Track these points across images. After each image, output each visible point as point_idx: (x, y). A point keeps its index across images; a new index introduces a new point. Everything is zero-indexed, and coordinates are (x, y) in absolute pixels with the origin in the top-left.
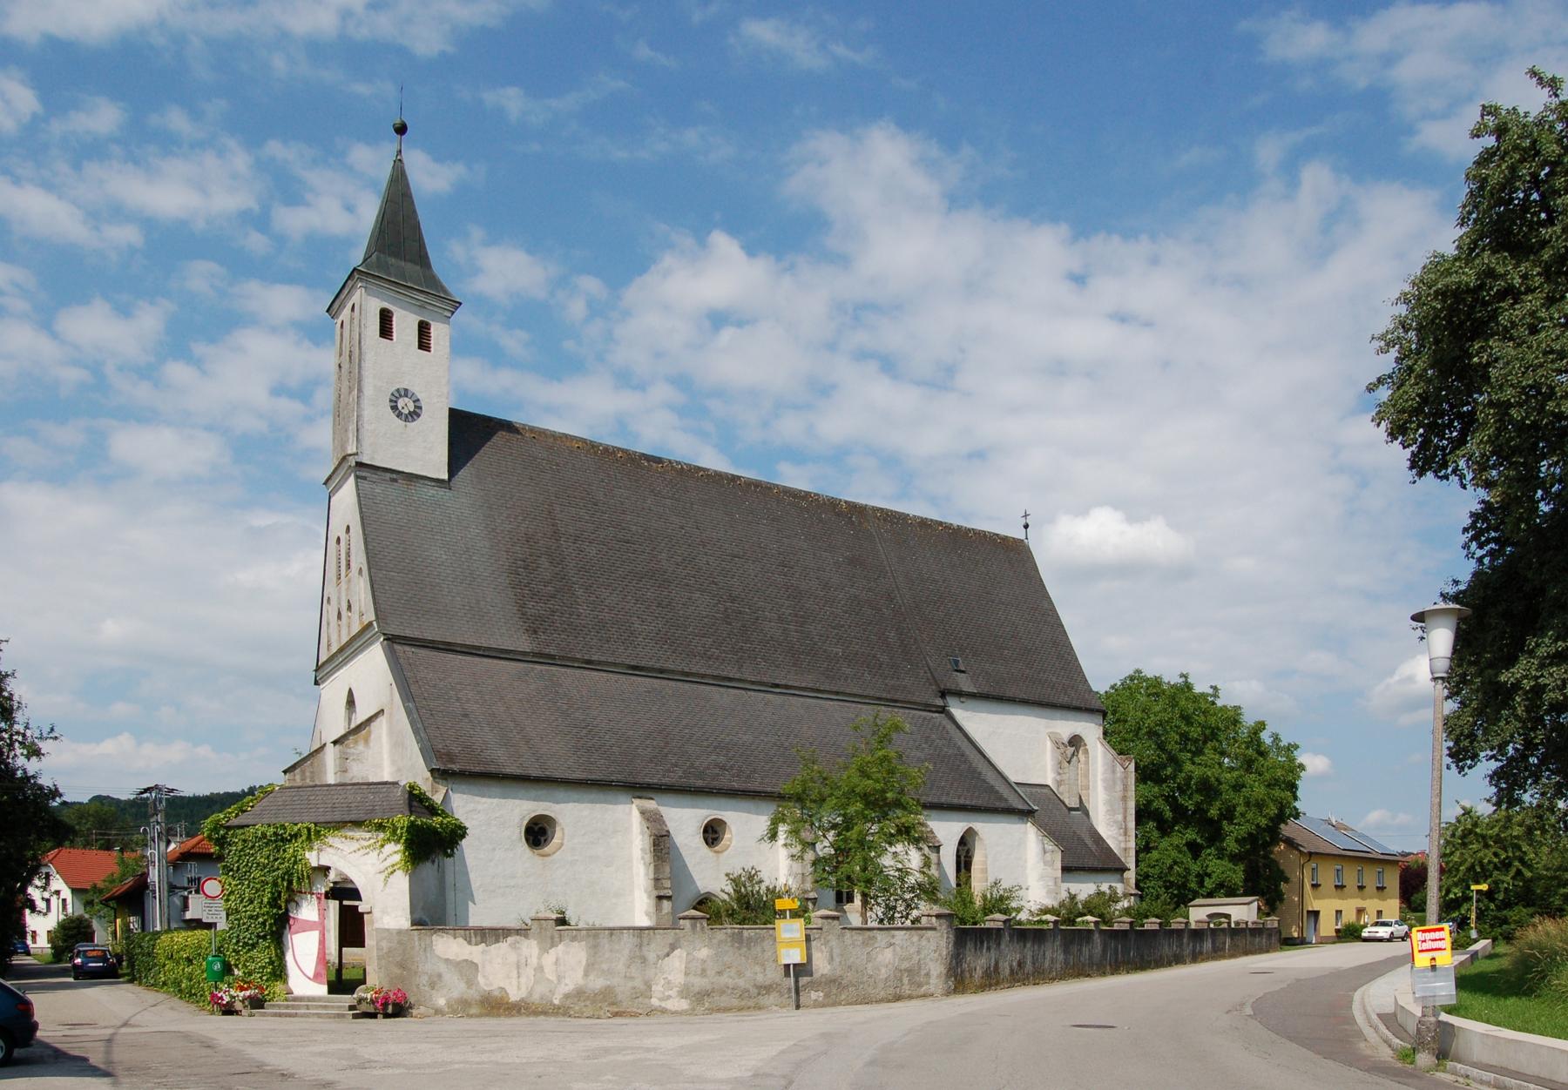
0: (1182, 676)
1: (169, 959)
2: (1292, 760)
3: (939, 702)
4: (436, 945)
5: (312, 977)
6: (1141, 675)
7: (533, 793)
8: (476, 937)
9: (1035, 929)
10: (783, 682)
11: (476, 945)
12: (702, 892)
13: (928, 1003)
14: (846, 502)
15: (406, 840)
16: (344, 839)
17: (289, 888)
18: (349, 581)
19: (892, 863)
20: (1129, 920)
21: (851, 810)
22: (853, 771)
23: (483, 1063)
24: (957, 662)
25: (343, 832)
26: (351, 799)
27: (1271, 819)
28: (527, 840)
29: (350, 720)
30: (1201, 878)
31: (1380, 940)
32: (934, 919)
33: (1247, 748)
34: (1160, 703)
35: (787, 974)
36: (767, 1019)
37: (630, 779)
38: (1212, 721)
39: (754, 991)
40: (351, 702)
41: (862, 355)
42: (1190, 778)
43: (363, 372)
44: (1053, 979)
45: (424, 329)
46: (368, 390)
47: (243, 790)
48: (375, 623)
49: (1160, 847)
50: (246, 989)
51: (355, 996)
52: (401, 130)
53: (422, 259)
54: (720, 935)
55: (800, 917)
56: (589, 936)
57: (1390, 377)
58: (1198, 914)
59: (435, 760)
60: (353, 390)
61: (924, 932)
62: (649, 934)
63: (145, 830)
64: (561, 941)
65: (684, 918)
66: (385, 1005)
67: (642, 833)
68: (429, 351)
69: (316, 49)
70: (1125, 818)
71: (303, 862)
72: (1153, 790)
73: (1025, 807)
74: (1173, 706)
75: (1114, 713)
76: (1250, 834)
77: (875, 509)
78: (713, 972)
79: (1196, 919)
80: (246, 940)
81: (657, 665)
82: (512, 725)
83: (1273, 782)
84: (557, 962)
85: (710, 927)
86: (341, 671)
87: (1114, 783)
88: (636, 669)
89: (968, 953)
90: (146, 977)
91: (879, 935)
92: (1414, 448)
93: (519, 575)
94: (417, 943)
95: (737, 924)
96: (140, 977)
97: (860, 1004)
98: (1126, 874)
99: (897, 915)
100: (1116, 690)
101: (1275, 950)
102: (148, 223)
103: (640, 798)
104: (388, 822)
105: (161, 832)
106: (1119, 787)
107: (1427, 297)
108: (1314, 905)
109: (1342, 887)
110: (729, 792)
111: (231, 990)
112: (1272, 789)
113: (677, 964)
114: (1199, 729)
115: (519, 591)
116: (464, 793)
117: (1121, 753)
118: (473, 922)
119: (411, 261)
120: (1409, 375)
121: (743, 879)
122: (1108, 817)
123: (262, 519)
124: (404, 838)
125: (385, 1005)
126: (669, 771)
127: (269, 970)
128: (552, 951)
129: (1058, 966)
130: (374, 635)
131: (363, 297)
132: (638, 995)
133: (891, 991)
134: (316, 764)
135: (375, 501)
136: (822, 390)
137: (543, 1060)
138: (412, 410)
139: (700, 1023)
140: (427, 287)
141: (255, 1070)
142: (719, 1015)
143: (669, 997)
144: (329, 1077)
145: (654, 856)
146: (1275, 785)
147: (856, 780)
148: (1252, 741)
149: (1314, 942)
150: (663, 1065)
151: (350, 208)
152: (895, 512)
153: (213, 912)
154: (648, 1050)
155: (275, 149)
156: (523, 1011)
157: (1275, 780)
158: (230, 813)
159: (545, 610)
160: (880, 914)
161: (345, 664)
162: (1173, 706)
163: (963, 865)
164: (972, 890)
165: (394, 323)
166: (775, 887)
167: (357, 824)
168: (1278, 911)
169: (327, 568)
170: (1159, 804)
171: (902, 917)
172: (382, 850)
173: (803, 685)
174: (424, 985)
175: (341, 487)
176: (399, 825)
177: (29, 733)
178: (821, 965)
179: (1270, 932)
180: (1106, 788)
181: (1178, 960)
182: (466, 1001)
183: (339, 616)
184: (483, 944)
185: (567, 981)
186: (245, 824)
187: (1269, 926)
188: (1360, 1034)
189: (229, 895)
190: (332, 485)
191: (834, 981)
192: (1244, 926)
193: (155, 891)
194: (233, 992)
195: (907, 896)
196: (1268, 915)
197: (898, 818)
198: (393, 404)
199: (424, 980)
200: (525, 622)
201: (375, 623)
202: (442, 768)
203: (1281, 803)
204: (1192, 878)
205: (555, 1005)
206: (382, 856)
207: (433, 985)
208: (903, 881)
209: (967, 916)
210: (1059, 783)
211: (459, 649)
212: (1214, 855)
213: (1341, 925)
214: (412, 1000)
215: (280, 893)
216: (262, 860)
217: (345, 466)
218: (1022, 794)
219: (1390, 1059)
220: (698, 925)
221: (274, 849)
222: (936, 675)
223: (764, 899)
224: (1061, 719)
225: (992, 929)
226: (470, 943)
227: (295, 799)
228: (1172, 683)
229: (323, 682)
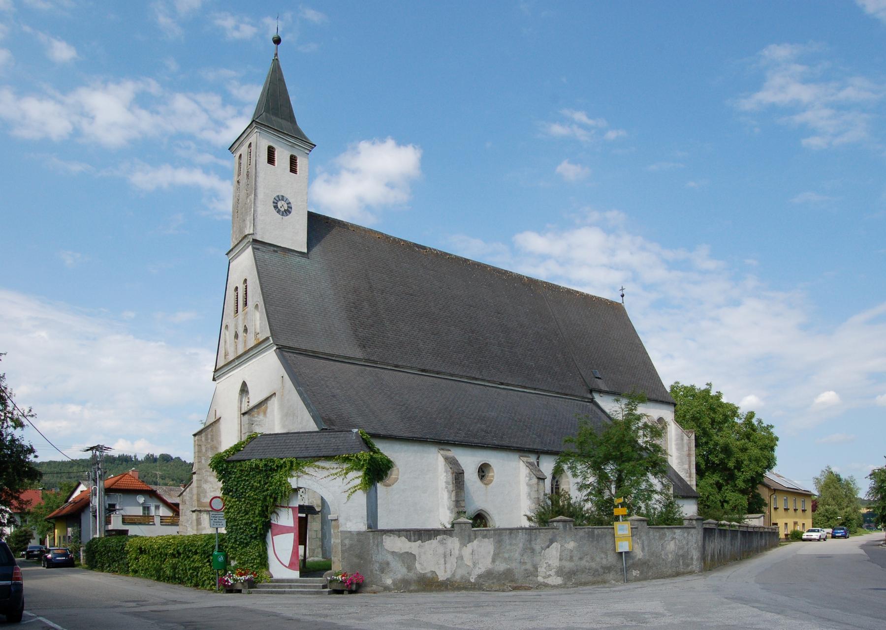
3: (589, 396)
4: (385, 542)
5: (287, 565)
10: (506, 382)
11: (415, 541)
14: (527, 277)
15: (367, 468)
16: (317, 470)
39: (601, 570)
40: (244, 389)
43: (258, 184)
45: (293, 161)
46: (261, 196)
48: (271, 338)
53: (291, 118)
54: (581, 533)
56: (495, 534)
62: (536, 532)
64: (475, 538)
67: (446, 472)
68: (296, 174)
71: (286, 485)
76: (752, 477)
78: (577, 558)
80: (242, 540)
81: (436, 369)
83: (763, 447)
87: (683, 446)
93: (352, 312)
94: (371, 541)
97: (659, 578)
103: (443, 449)
106: (686, 448)
112: (763, 451)
115: (353, 321)
119: (284, 119)
122: (679, 466)
127: (258, 561)
128: (469, 545)
133: (674, 569)
134: (214, 431)
135: (265, 263)
138: (286, 209)
143: (550, 576)
146: (764, 449)
153: (217, 521)
159: (369, 334)
165: (276, 155)
167: (328, 458)
169: (225, 307)
177: (15, 412)
180: (678, 449)
183: (236, 336)
184: (420, 541)
185: (480, 566)
186: (242, 459)
189: (229, 509)
190: (232, 255)
191: (645, 563)
198: (275, 205)
199: (376, 566)
200: (358, 341)
201: (271, 338)
207: (382, 570)
212: (730, 490)
214: (367, 580)
215: (267, 507)
217: (246, 241)
224: (653, 408)
226: (410, 540)
227: (274, 442)
229: (218, 379)
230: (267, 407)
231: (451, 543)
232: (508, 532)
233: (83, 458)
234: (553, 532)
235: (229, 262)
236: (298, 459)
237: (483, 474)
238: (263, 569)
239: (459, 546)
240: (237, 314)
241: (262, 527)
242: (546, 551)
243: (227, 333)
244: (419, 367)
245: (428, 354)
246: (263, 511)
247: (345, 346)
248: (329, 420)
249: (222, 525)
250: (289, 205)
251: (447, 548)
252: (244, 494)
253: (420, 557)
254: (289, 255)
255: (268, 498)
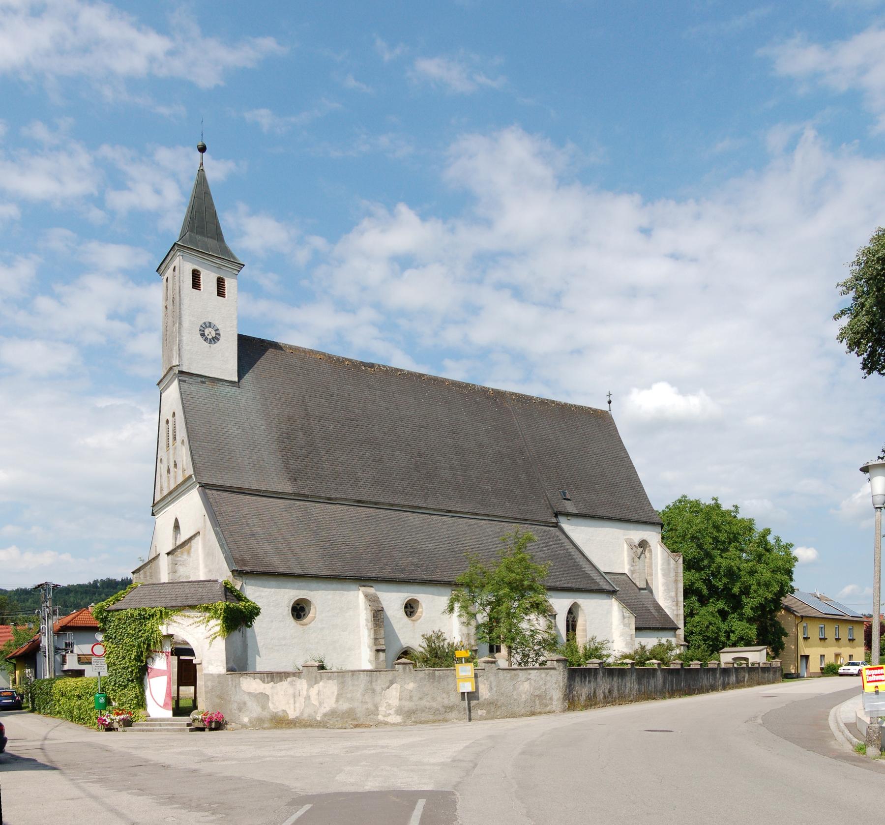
0: (714, 499)
1: (63, 696)
2: (789, 554)
3: (554, 520)
4: (242, 684)
6: (686, 499)
7: (297, 584)
8: (267, 678)
9: (619, 669)
10: (454, 509)
11: (268, 683)
12: (404, 647)
13: (552, 717)
14: (492, 389)
15: (224, 617)
17: (148, 649)
18: (175, 448)
19: (528, 627)
20: (680, 662)
21: (501, 593)
22: (502, 567)
23: (283, 757)
24: (564, 494)
25: (183, 613)
26: (187, 591)
27: (775, 594)
28: (293, 615)
29: (176, 538)
30: (728, 634)
31: (852, 675)
32: (555, 662)
33: (758, 546)
34: (699, 517)
35: (463, 699)
36: (452, 727)
37: (358, 574)
38: (734, 529)
40: (177, 527)
41: (500, 286)
42: (720, 567)
43: (182, 312)
44: (631, 701)
45: (220, 283)
46: (186, 324)
47: (90, 583)
48: (193, 476)
49: (700, 613)
50: (121, 714)
51: (191, 717)
52: (203, 149)
53: (218, 236)
54: (421, 674)
55: (470, 662)
56: (338, 676)
57: (849, 310)
58: (726, 658)
59: (234, 565)
60: (176, 323)
61: (549, 671)
62: (377, 674)
63: (38, 612)
64: (321, 680)
65: (398, 664)
66: (210, 722)
67: (366, 609)
69: (133, 83)
70: (677, 594)
71: (157, 632)
72: (694, 575)
73: (611, 588)
74: (708, 520)
75: (669, 524)
76: (761, 604)
77: (512, 394)
79: (725, 661)
80: (120, 683)
81: (373, 500)
82: (282, 541)
83: (776, 569)
84: (319, 693)
85: (415, 669)
86: (170, 507)
88: (360, 503)
89: (576, 684)
90: (44, 708)
91: (520, 673)
92: (865, 355)
94: (230, 683)
95: (430, 667)
96: (39, 709)
97: (509, 717)
98: (678, 632)
99: (529, 660)
100: (670, 509)
101: (779, 682)
102: (24, 203)
103: (364, 586)
104: (212, 606)
105: (50, 613)
106: (672, 574)
107: (871, 262)
108: (805, 651)
109: (825, 639)
110: (420, 581)
111: (111, 715)
112: (776, 574)
113: (394, 693)
114: (725, 535)
116: (253, 586)
117: (673, 551)
118: (259, 669)
119: (211, 238)
120: (862, 308)
121: (433, 638)
122: (666, 594)
123: (103, 402)
124: (222, 616)
125: (210, 722)
126: (382, 568)
127: (135, 702)
128: (316, 686)
129: (635, 693)
130: (193, 483)
131: (181, 261)
132: (370, 713)
133: (528, 709)
135: (192, 396)
136: (473, 310)
137: (320, 754)
138: (214, 336)
139: (409, 731)
140: (222, 255)
141: (144, 763)
142: (421, 726)
143: (389, 714)
144: (194, 767)
145: (374, 624)
146: (777, 571)
147: (504, 573)
148: (761, 542)
149: (805, 676)
150: (395, 755)
151: (158, 192)
152: (524, 395)
154: (383, 747)
155: (106, 151)
156: (297, 725)
157: (777, 568)
158: (109, 602)
159: (302, 466)
160: (519, 659)
161: (173, 502)
162: (708, 520)
163: (570, 627)
164: (577, 644)
165: (201, 279)
166: (454, 643)
167: (192, 607)
168: (780, 656)
169: (159, 439)
170: (699, 585)
171: (533, 661)
172: (208, 623)
173: (466, 510)
174: (235, 710)
175: (169, 387)
176: (219, 608)
178: (484, 693)
179: (775, 670)
180: (664, 575)
181: (713, 688)
182: (261, 719)
183: (169, 471)
184: (272, 683)
185: (325, 705)
187: (774, 666)
188: (832, 736)
189: (109, 654)
190: (163, 385)
191: (492, 703)
192: (757, 666)
193: (46, 652)
194: (112, 717)
195: (536, 648)
196: (774, 658)
197: (531, 597)
199: (235, 706)
200: (288, 474)
201: (193, 476)
202: (239, 570)
203: (781, 583)
204: (722, 634)
205: (318, 720)
206: (208, 628)
207: (240, 710)
208: (534, 638)
209: (574, 661)
210: (633, 572)
211: (247, 492)
212: (736, 619)
213: (825, 665)
214: (227, 718)
215: (142, 652)
216: (131, 631)
217: (172, 373)
218: (609, 580)
219: (851, 751)
220: (407, 668)
221: (138, 624)
222: (552, 503)
223: (447, 651)
225: (592, 668)
226: (264, 682)
228: (707, 504)
229: (157, 514)
230: (191, 547)
231: (300, 684)
232: (350, 673)
233: (81, 583)
234: (394, 674)
235: (161, 393)
236: (167, 608)
237: (412, 610)
238: (140, 709)
239: (306, 687)
240: (175, 441)
241: (137, 670)
242: (386, 691)
243: (162, 466)
244: (354, 498)
245: (366, 484)
246: (139, 656)
247: (274, 480)
248: (243, 560)
249: (104, 669)
250: (217, 332)
251: (296, 689)
252: (122, 640)
253: (273, 697)
254: (218, 385)
255: (142, 644)
